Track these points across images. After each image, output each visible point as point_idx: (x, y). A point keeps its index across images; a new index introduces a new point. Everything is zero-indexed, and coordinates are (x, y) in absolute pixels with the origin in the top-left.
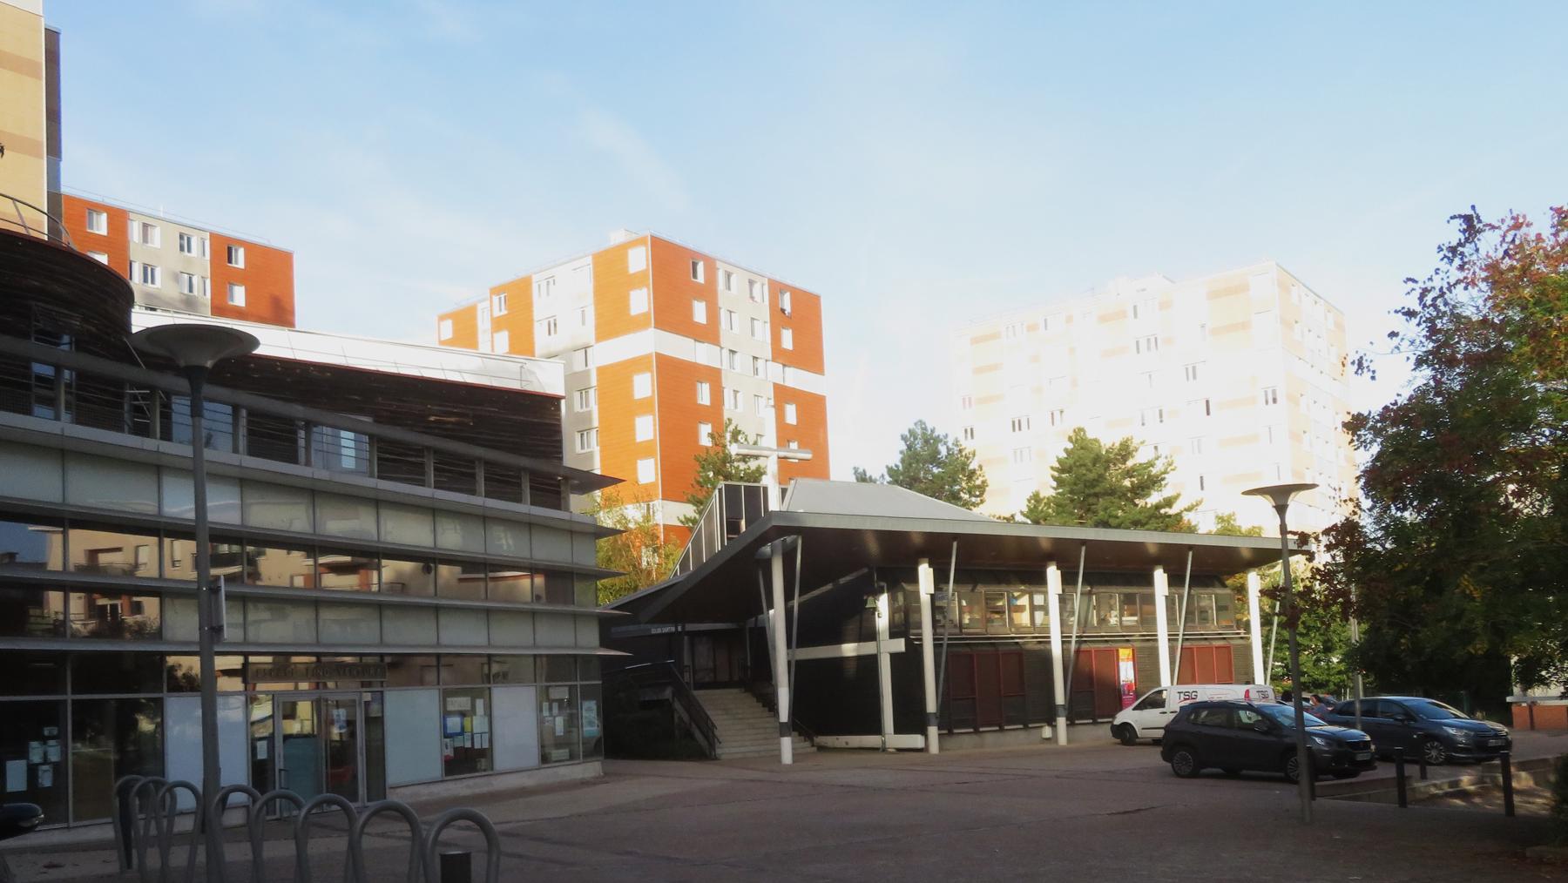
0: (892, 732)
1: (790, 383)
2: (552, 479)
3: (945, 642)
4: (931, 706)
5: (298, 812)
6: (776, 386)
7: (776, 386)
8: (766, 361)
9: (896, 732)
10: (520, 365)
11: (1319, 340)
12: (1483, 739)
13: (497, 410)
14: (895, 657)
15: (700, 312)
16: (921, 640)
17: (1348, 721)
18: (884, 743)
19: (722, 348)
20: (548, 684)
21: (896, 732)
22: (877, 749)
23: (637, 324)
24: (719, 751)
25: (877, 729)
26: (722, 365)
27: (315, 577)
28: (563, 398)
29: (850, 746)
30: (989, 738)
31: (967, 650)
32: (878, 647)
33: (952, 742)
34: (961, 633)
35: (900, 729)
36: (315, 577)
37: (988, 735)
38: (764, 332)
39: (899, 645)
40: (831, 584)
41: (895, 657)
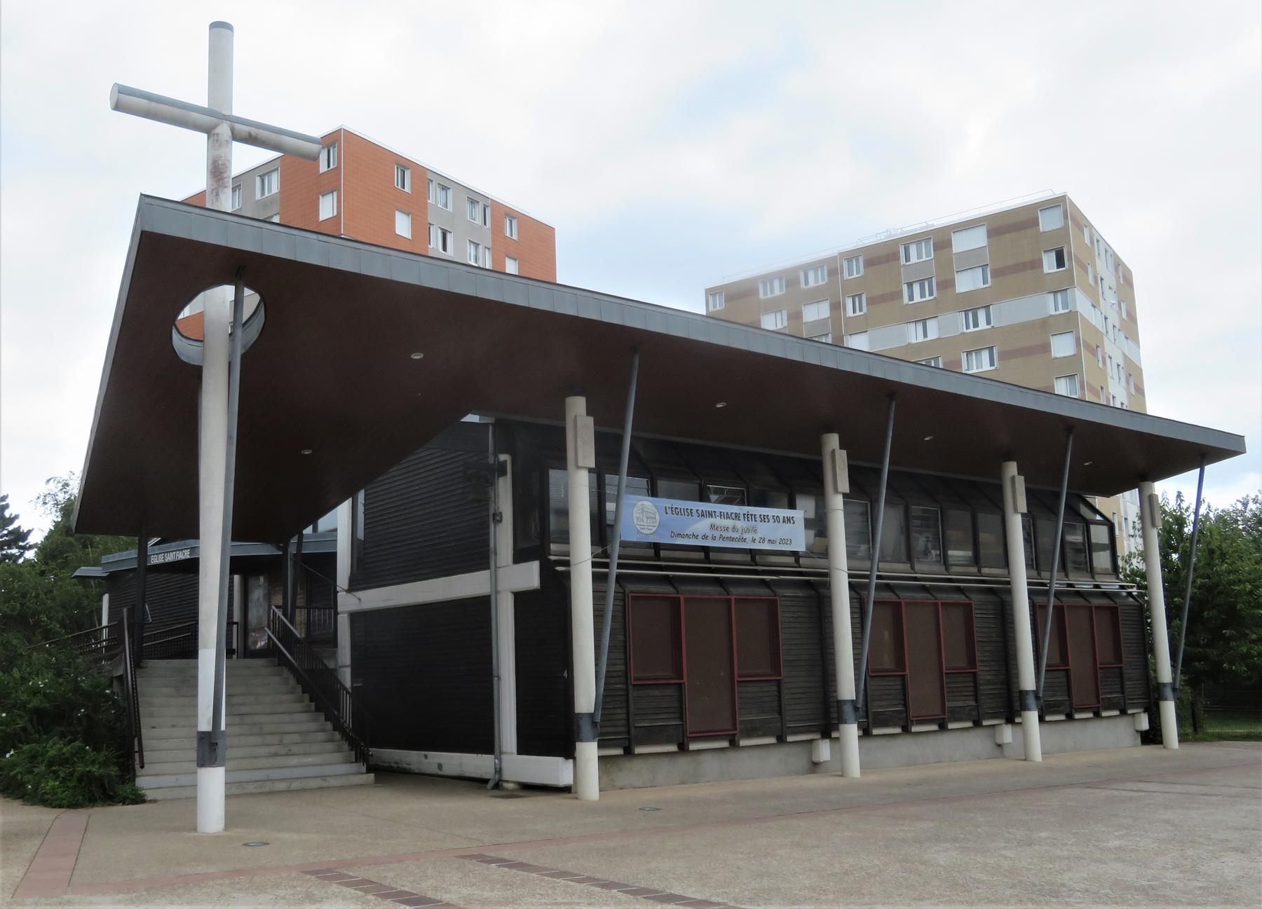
0: (516, 753)
3: (615, 571)
4: (1028, 679)
12: (1256, 790)
14: (521, 598)
16: (567, 563)
18: (499, 771)
20: (775, 598)
22: (483, 781)
24: (144, 782)
25: (485, 743)
27: (1051, 393)
29: (447, 771)
30: (710, 764)
31: (763, 592)
32: (494, 581)
33: (633, 772)
34: (755, 563)
35: (527, 745)
36: (1051, 393)
37: (707, 758)
39: (529, 576)
41: (521, 598)
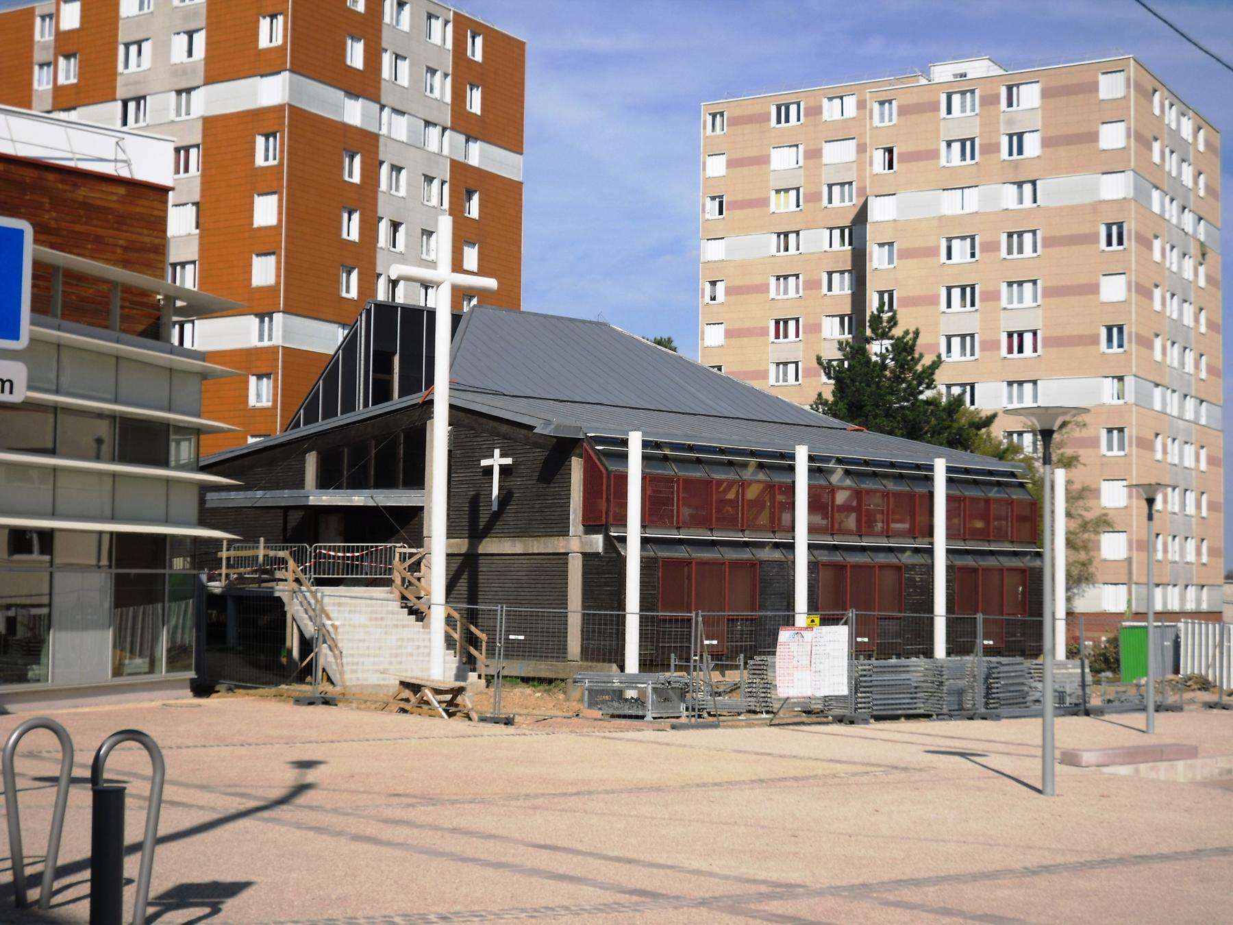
1: (474, 160)
2: (148, 296)
5: (1145, 679)
6: (454, 164)
7: (454, 164)
8: (444, 129)
9: (17, 338)
10: (117, 139)
11: (581, 715)
13: (639, 685)
15: (356, 55)
17: (157, 664)
19: (382, 107)
21: (17, 338)
23: (266, 65)
26: (380, 129)
28: (172, 189)
38: (443, 89)
40: (511, 459)
41: (587, 557)
